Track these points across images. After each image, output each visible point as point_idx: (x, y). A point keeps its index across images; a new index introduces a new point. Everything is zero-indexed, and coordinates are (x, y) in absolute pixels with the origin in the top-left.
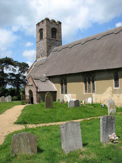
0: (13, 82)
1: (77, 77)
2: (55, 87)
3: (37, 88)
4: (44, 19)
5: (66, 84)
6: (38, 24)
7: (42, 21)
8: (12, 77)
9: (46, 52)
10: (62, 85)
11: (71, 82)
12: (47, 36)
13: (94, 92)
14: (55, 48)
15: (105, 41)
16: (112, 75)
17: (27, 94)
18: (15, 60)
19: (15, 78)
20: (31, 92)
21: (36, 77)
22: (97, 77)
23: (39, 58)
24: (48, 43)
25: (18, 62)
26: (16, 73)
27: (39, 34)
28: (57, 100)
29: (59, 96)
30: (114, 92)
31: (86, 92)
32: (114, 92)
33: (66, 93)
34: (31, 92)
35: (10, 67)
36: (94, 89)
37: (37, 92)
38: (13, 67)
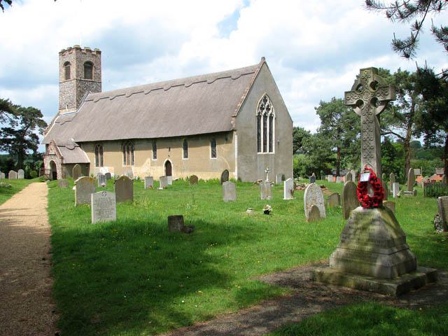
0: (10, 145)
1: (145, 143)
2: (87, 157)
3: (62, 158)
4: (66, 49)
5: (102, 154)
6: (62, 53)
7: (70, 49)
8: (7, 135)
9: (75, 101)
10: (97, 154)
11: (108, 150)
13: (133, 164)
14: (91, 95)
15: (151, 100)
16: (151, 145)
17: (48, 166)
18: (15, 102)
19: (13, 137)
20: (53, 164)
21: (59, 143)
22: (136, 146)
23: (64, 110)
24: (78, 87)
25: (22, 107)
26: (17, 128)
27: (64, 71)
28: (90, 175)
29: (96, 171)
30: (153, 163)
31: (125, 164)
32: (153, 163)
33: (102, 165)
34: (53, 164)
35: (6, 117)
37: (62, 164)
38: (11, 116)
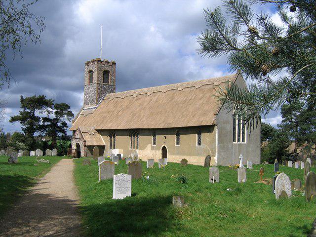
2: (103, 140)
5: (114, 137)
7: (93, 61)
12: (97, 81)
13: (137, 148)
17: (74, 147)
19: (49, 123)
20: (78, 145)
24: (98, 89)
31: (131, 148)
33: (114, 148)
34: (78, 145)
36: (114, 145)
37: (85, 146)
